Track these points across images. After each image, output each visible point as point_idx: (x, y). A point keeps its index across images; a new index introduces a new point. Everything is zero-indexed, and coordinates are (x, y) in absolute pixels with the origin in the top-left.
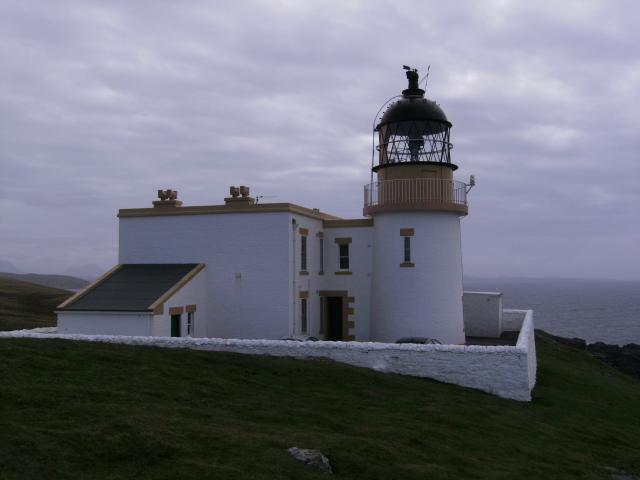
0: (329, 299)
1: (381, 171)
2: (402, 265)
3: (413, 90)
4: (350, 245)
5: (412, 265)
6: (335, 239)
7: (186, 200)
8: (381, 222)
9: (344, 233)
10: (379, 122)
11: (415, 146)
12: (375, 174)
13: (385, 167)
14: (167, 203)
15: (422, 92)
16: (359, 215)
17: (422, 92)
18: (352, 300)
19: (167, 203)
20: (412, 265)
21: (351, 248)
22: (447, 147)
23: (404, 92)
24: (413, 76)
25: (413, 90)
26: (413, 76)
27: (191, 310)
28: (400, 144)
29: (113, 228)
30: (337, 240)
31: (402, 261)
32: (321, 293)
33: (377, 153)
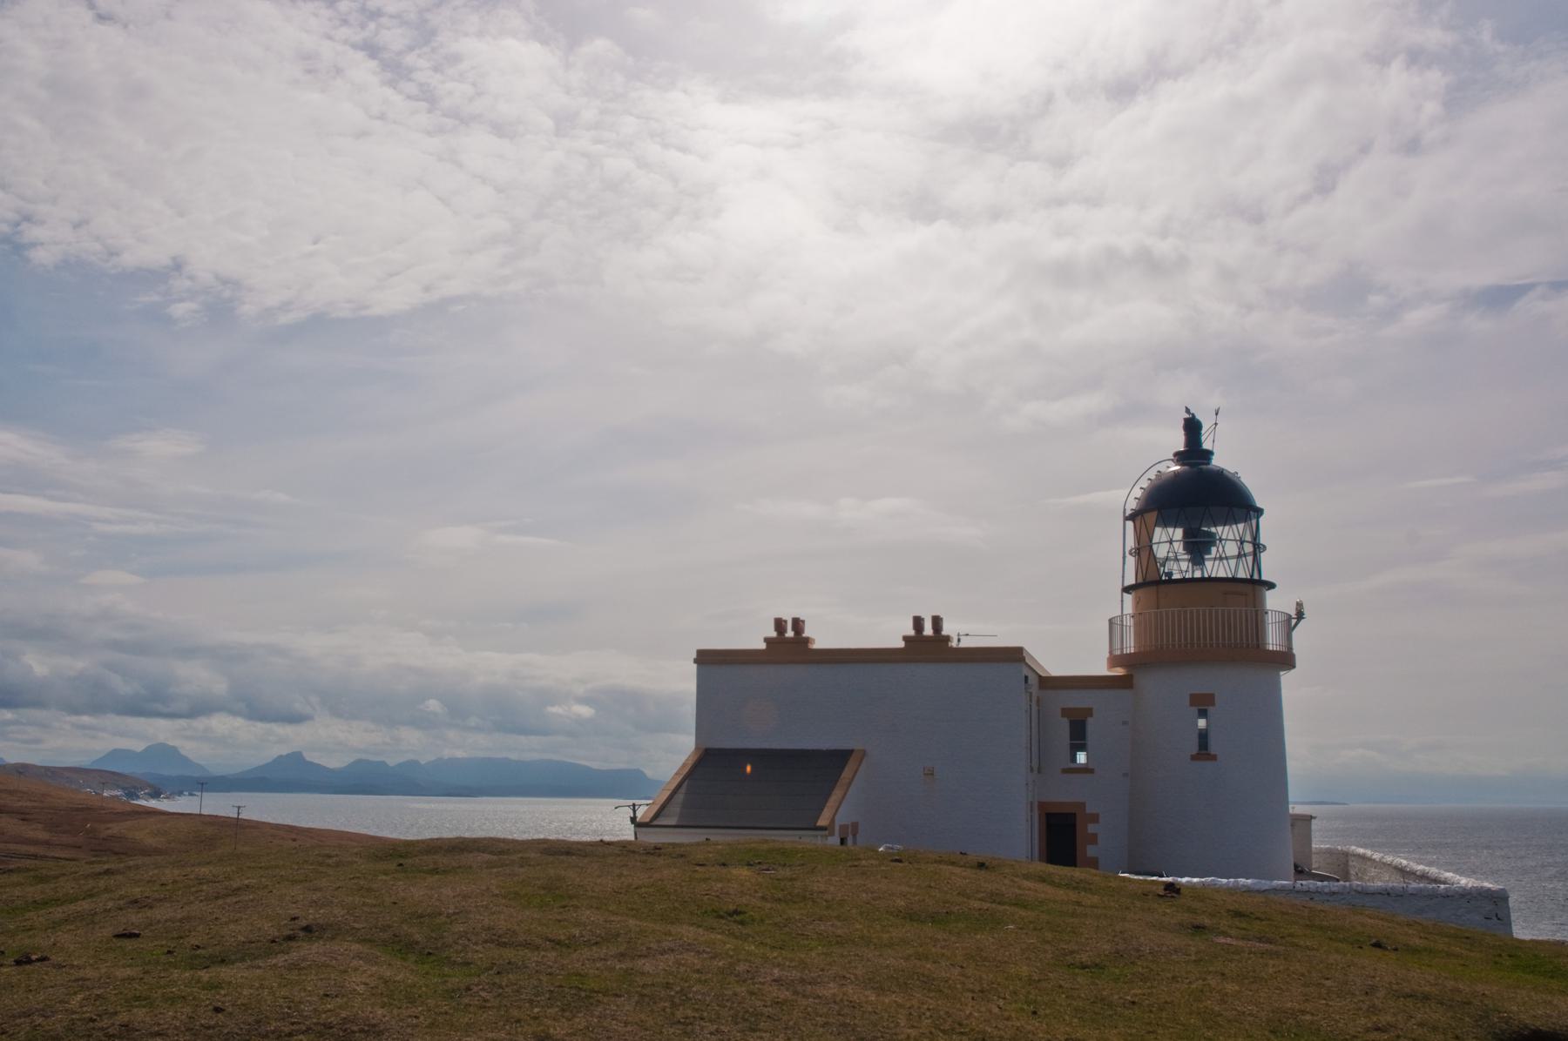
0: (1049, 816)
1: (1141, 592)
2: (1193, 758)
3: (1194, 451)
4: (1090, 721)
5: (1214, 758)
6: (1068, 708)
8: (1152, 685)
9: (1076, 700)
10: (1132, 505)
11: (1198, 547)
12: (1129, 598)
13: (1150, 583)
14: (789, 645)
15: (1209, 453)
16: (1100, 668)
17: (1209, 453)
18: (1095, 818)
20: (1214, 758)
21: (1091, 724)
23: (1177, 454)
24: (1192, 427)
25: (1194, 451)
26: (1192, 427)
27: (855, 826)
28: (1168, 541)
29: (683, 681)
30: (1066, 712)
31: (1195, 750)
32: (1042, 805)
33: (1131, 561)
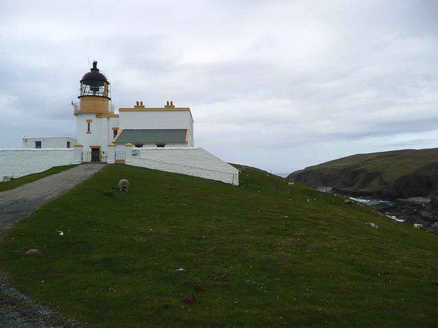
3: (95, 69)
7: (147, 106)
19: (140, 107)
22: (107, 90)
24: (95, 64)
25: (95, 69)
26: (95, 64)
